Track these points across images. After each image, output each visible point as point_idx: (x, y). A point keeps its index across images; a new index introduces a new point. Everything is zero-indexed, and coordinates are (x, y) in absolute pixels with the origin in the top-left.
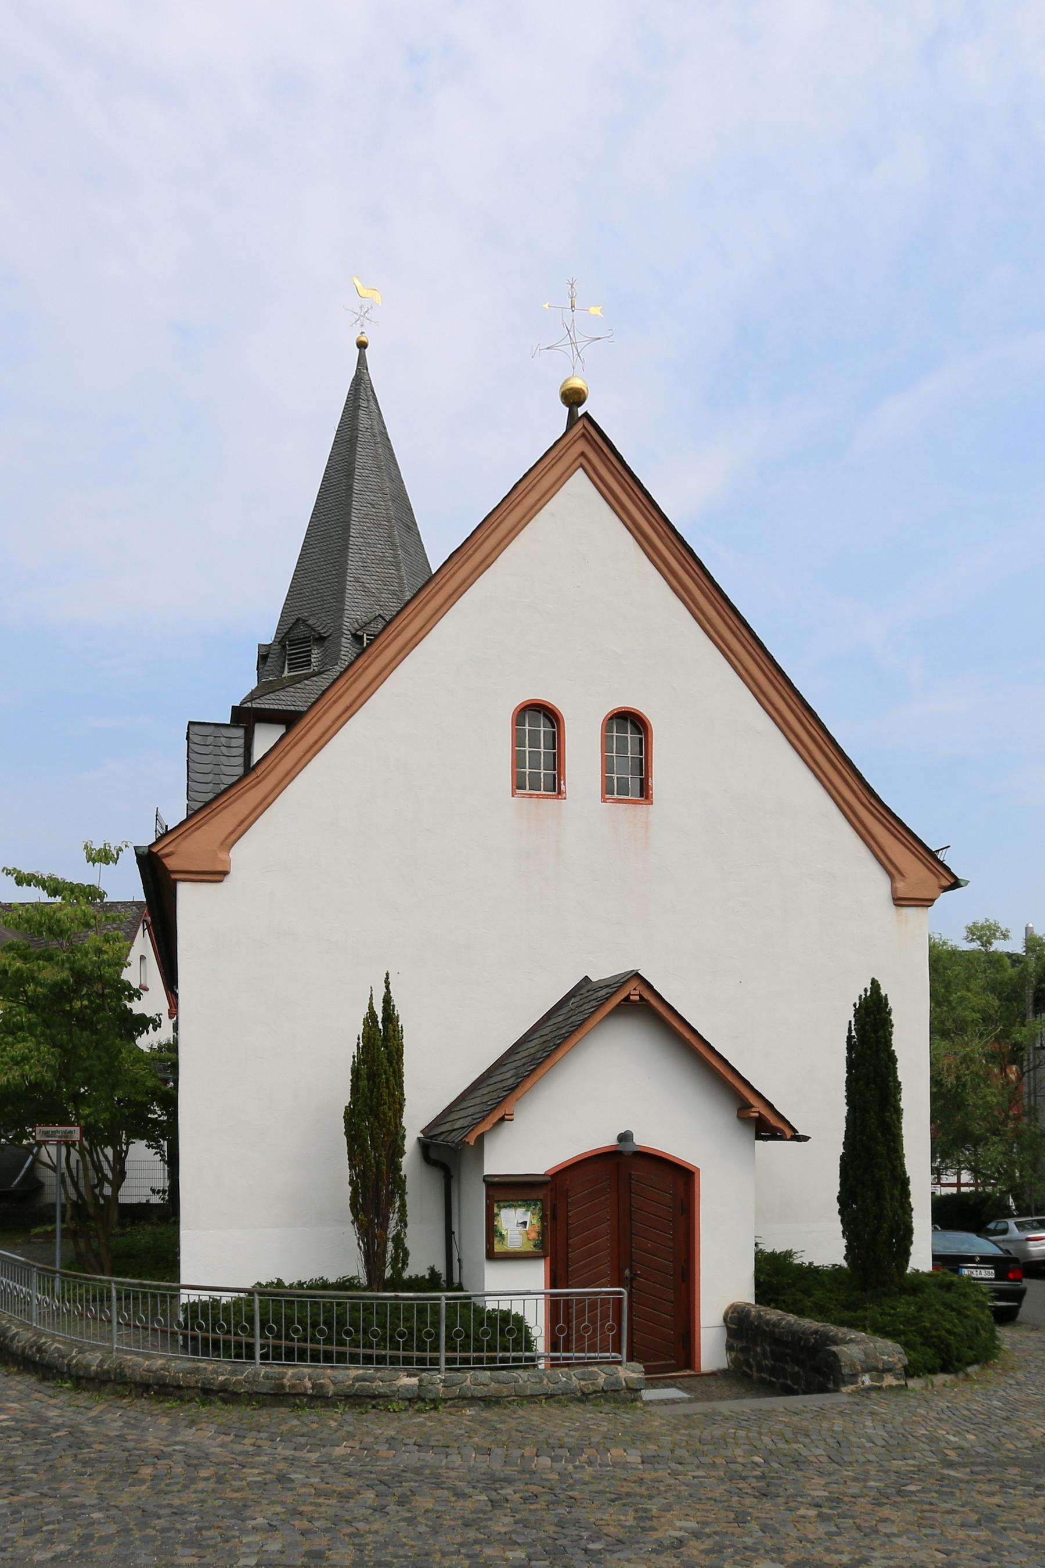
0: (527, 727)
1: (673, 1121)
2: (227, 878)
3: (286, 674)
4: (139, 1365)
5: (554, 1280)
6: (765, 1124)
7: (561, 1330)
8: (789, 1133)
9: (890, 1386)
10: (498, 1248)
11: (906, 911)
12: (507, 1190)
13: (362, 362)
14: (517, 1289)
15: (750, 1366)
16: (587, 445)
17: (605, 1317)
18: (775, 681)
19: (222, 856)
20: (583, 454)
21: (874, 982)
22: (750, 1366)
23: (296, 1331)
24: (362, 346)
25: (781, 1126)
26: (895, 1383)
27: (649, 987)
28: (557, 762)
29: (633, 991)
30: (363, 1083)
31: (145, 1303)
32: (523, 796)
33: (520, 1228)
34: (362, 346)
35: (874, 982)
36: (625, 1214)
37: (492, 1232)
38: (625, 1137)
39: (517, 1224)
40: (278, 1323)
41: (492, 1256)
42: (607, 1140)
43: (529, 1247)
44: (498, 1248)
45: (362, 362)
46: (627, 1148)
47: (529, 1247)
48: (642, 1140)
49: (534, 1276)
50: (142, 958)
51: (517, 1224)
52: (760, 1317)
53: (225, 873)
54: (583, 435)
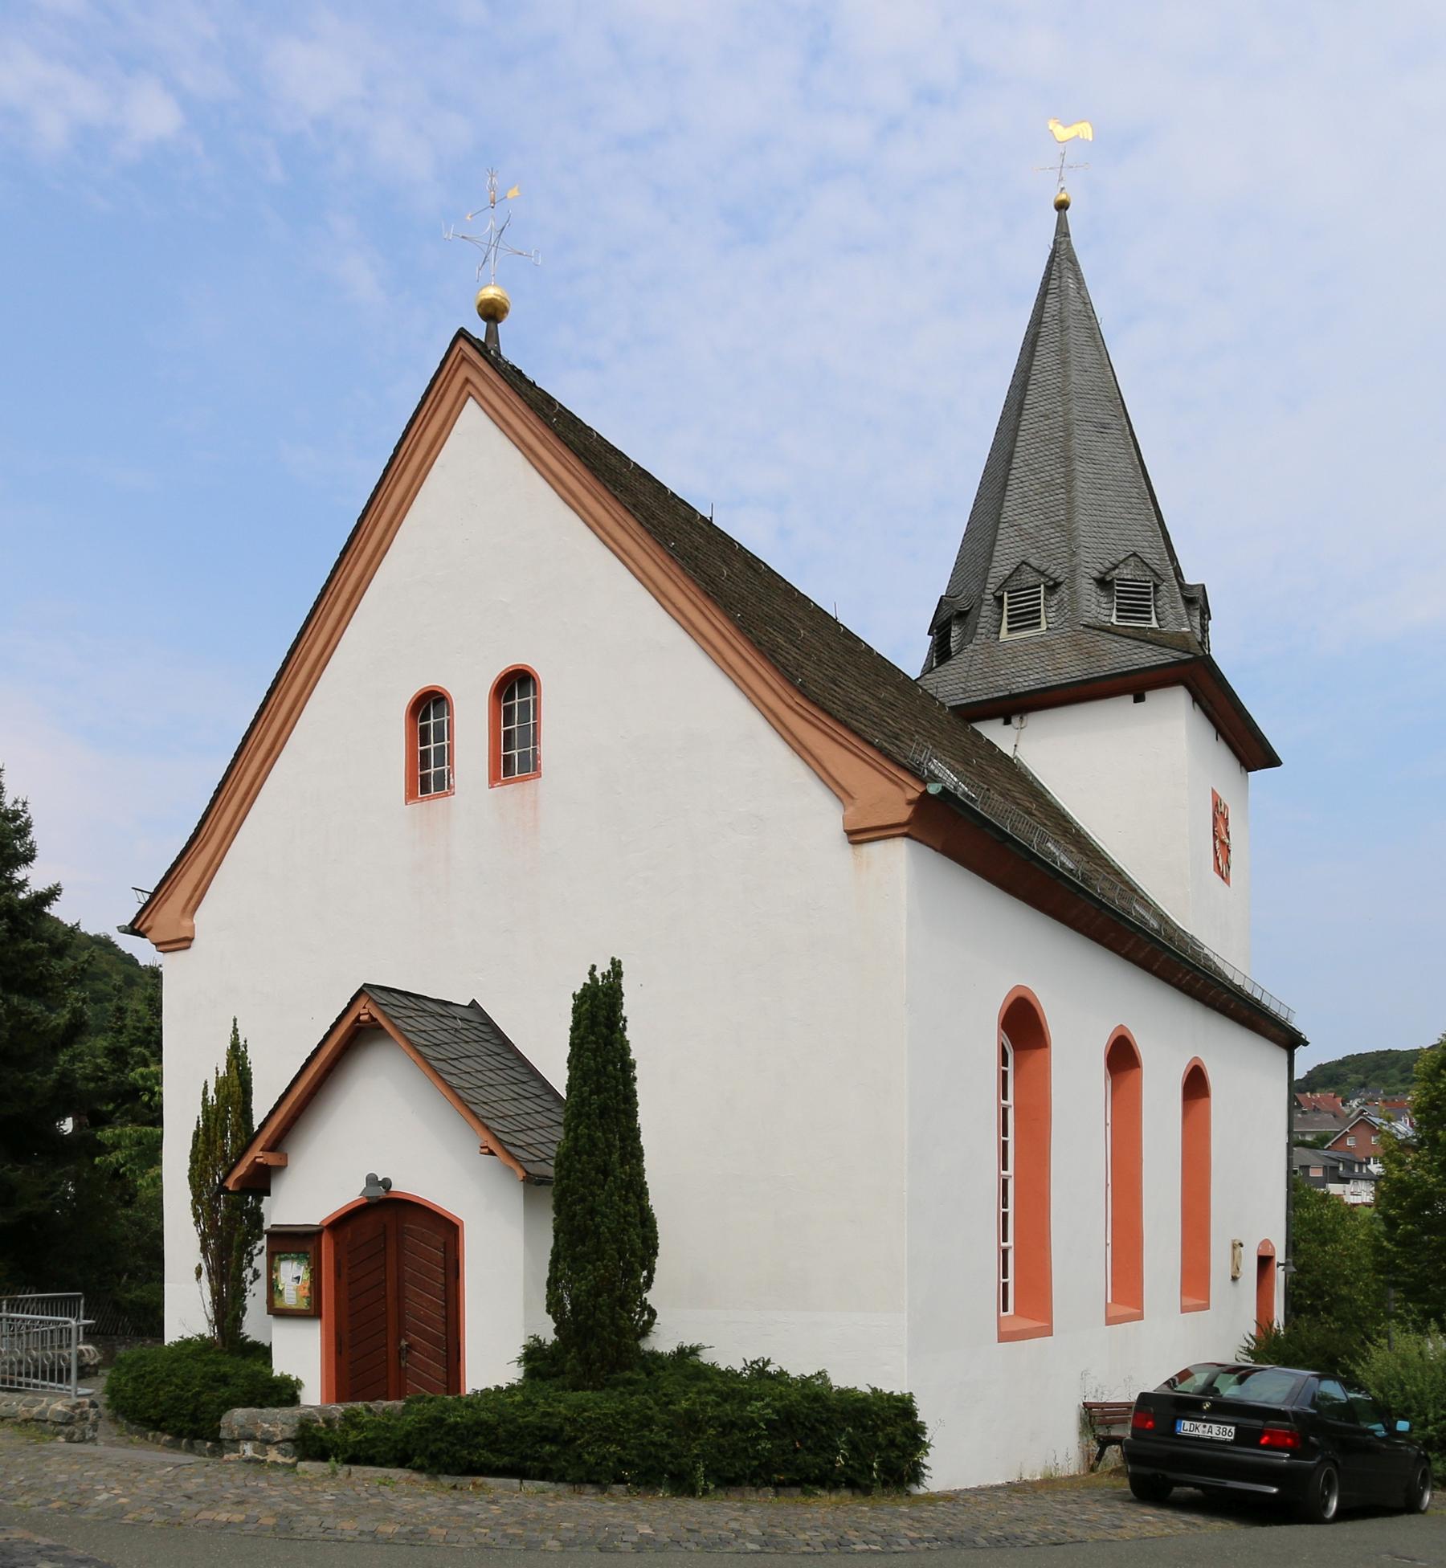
0: (432, 720)
2: (194, 943)
4: (395, 1407)
9: (275, 1462)
10: (278, 1304)
11: (867, 849)
13: (1062, 230)
16: (479, 363)
19: (186, 923)
20: (467, 381)
21: (616, 964)
24: (1062, 206)
26: (281, 1459)
30: (200, 1146)
31: (28, 1368)
33: (295, 1284)
34: (1062, 206)
35: (616, 964)
37: (273, 1288)
39: (292, 1276)
43: (303, 1305)
44: (278, 1304)
45: (1062, 230)
47: (303, 1305)
51: (292, 1276)
53: (191, 940)
54: (463, 359)
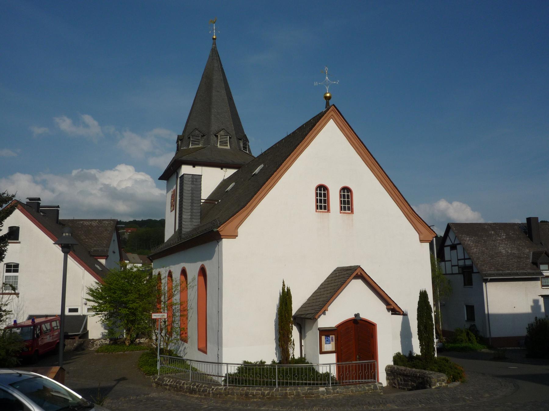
1: (372, 310)
3: (190, 147)
5: (338, 360)
6: (394, 310)
7: (341, 375)
8: (402, 313)
12: (325, 332)
14: (327, 363)
15: (395, 384)
17: (352, 370)
18: (360, 149)
22: (395, 384)
23: (289, 376)
25: (399, 310)
27: (363, 270)
28: (327, 201)
29: (358, 271)
32: (319, 212)
36: (357, 338)
38: (357, 315)
40: (260, 374)
41: (322, 352)
42: (353, 316)
44: (323, 351)
46: (357, 318)
48: (362, 316)
49: (332, 358)
50: (114, 240)
52: (398, 369)
